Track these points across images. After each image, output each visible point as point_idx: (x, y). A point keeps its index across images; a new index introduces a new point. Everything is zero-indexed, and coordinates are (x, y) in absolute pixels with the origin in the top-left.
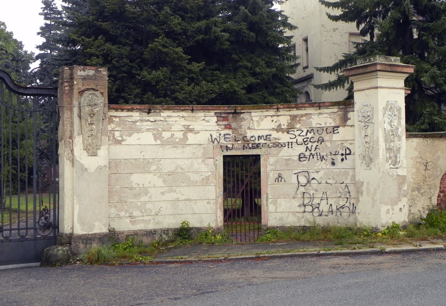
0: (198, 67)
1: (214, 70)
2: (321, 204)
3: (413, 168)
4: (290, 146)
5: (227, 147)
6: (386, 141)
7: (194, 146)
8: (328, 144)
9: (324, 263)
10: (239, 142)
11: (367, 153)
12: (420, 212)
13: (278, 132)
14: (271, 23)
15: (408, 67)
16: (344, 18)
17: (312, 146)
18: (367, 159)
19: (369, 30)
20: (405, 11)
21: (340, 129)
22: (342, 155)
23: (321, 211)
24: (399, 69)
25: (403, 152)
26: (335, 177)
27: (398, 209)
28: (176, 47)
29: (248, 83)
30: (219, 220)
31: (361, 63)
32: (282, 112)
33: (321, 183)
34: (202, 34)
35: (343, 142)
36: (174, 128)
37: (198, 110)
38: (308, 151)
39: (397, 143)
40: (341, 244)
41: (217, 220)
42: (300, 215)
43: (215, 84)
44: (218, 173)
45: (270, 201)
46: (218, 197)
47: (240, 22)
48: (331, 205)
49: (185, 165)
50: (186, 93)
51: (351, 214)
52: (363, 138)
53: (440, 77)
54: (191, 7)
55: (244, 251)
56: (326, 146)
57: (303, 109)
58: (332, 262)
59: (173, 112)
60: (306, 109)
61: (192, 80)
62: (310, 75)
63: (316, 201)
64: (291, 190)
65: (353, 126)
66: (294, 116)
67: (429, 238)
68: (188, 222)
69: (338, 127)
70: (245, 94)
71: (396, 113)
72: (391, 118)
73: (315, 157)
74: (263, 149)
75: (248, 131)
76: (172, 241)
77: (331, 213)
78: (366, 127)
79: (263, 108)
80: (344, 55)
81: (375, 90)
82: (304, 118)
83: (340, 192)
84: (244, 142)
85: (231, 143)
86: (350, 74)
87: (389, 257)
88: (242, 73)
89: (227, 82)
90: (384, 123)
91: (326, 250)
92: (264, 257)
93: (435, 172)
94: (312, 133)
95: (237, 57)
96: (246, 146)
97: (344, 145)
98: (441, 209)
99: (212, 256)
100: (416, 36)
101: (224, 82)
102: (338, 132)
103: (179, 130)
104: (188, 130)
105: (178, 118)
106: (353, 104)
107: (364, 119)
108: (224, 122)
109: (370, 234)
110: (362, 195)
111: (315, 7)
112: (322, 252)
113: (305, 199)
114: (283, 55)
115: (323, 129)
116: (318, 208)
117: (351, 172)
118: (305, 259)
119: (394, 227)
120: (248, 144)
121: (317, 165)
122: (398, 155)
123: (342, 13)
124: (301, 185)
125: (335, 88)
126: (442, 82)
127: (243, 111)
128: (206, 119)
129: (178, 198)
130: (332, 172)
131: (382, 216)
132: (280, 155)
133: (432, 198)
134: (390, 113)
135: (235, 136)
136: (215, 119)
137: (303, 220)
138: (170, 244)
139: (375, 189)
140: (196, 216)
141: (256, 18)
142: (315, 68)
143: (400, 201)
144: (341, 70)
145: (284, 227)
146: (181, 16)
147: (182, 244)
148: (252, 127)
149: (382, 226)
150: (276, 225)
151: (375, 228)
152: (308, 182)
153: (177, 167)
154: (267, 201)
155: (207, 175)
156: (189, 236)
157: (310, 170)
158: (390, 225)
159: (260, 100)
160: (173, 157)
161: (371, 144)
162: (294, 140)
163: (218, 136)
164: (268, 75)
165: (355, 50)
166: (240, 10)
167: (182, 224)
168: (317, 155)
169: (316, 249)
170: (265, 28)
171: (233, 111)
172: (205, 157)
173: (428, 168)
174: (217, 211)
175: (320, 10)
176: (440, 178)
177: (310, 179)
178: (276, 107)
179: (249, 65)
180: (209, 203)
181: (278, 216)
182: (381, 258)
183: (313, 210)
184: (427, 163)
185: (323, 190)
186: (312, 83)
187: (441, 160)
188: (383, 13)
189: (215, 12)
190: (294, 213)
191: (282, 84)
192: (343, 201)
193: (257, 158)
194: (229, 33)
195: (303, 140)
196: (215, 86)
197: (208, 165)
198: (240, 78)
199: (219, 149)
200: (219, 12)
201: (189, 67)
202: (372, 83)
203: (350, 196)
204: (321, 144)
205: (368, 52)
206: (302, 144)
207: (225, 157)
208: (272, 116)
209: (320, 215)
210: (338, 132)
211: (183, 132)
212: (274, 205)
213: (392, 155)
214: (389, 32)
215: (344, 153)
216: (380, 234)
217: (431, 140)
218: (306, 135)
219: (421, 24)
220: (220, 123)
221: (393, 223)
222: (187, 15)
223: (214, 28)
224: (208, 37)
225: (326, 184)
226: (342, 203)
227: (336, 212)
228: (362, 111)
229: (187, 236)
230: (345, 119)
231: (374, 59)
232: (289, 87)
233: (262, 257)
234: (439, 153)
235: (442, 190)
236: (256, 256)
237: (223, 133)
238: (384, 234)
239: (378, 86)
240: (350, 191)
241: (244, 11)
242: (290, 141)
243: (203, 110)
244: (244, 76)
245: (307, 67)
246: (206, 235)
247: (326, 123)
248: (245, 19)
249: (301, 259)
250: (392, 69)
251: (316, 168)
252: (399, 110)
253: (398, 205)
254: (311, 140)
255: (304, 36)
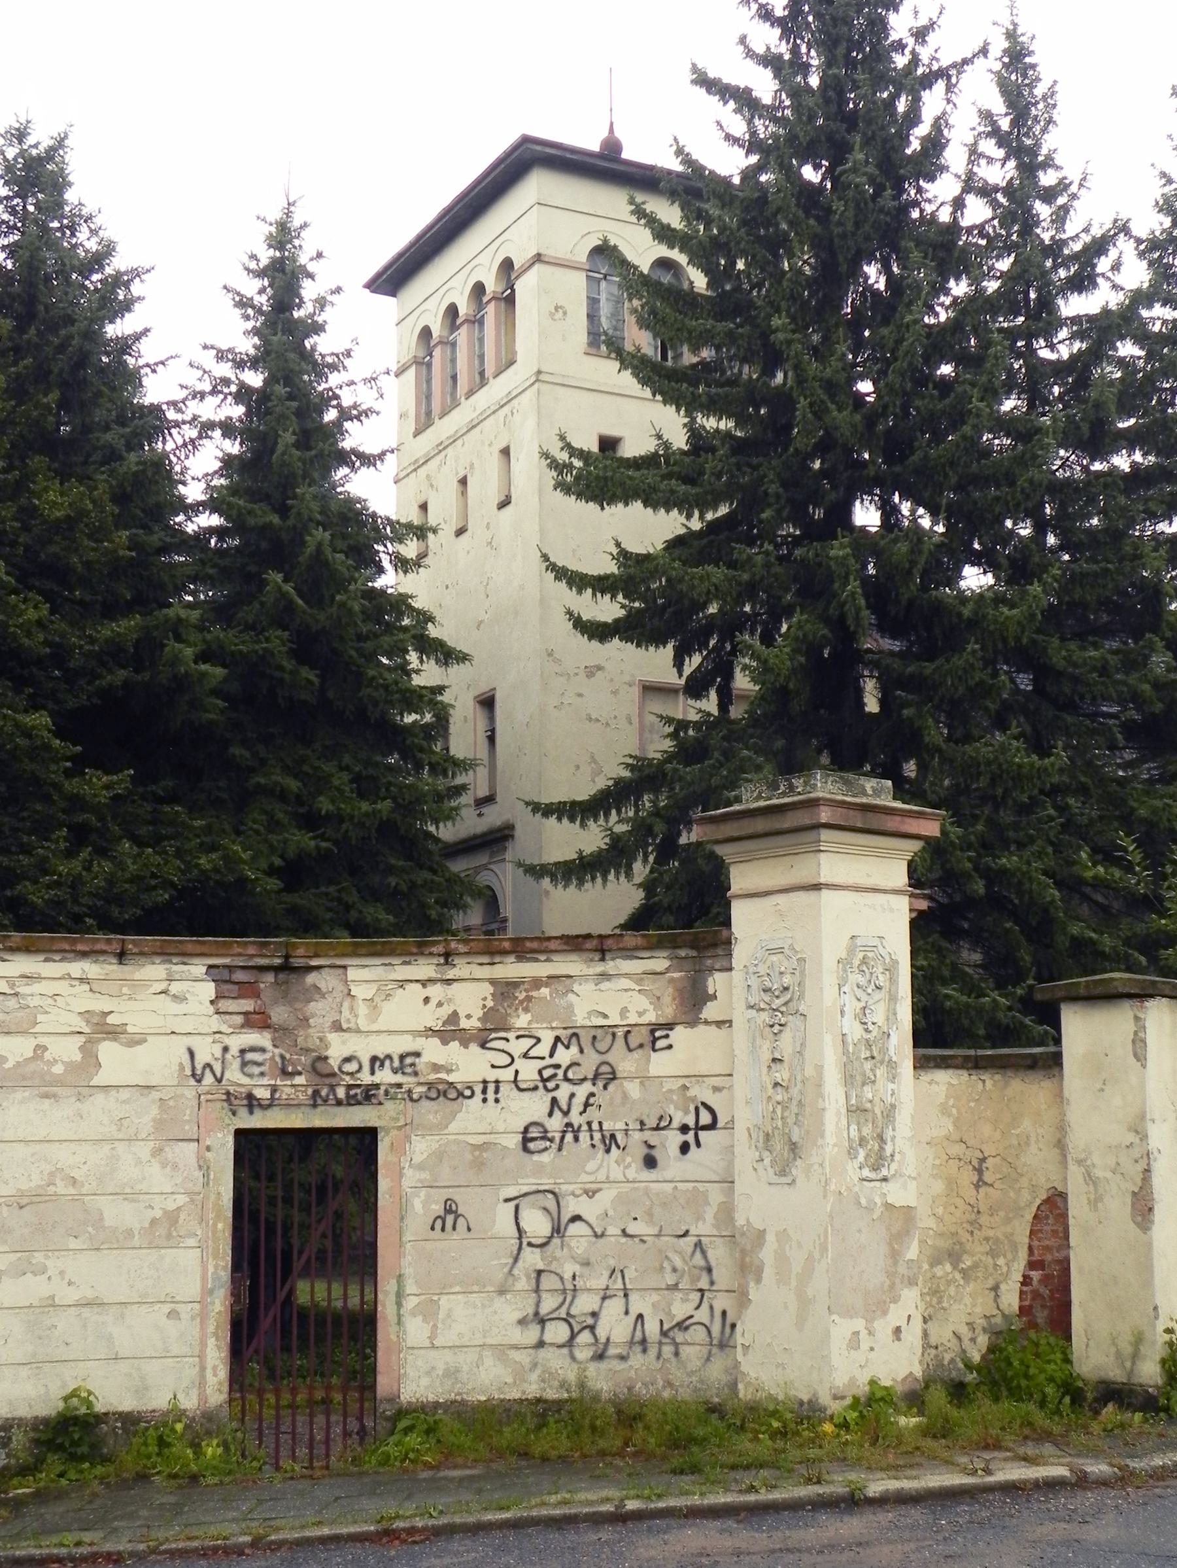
0: (107, 787)
1: (161, 800)
2: (603, 1314)
3: (934, 1176)
4: (491, 1095)
5: (250, 1097)
6: (848, 1079)
7: (125, 1094)
8: (633, 1089)
9: (652, 1553)
10: (300, 1080)
11: (780, 1123)
12: (959, 1338)
13: (445, 1042)
14: (376, 636)
15: (920, 815)
16: (628, 629)
17: (572, 1095)
18: (778, 1144)
19: (713, 678)
20: (842, 618)
21: (679, 1035)
22: (684, 1129)
23: (603, 1340)
24: (892, 823)
25: (904, 1118)
26: (657, 1210)
27: (889, 1332)
28: (26, 711)
29: (291, 852)
30: (211, 1380)
31: (759, 797)
32: (461, 968)
33: (603, 1235)
34: (124, 667)
35: (686, 1082)
36: (46, 1023)
37: (142, 954)
38: (557, 1114)
39: (884, 1087)
40: (695, 1469)
41: (202, 1384)
42: (523, 1357)
43: (166, 853)
44: (213, 1197)
45: (410, 1303)
46: (211, 1292)
47: (263, 630)
48: (640, 1316)
49: (85, 1168)
50: (58, 884)
51: (715, 1350)
52: (765, 1070)
53: (962, 850)
54: (88, 564)
55: (326, 1506)
56: (625, 1096)
57: (542, 957)
58: (678, 1548)
59: (46, 960)
60: (555, 957)
61: (80, 836)
62: (500, 829)
63: (584, 1304)
64: (494, 1263)
65: (723, 1022)
66: (508, 984)
67: (1008, 1440)
68: (90, 1393)
69: (670, 1026)
70: (279, 892)
71: (881, 978)
72: (864, 997)
73: (584, 1136)
74: (389, 1105)
75: (333, 1037)
76: (25, 1471)
77: (638, 1349)
78: (777, 1028)
79: (392, 953)
80: (630, 761)
81: (811, 896)
82: (545, 991)
83: (674, 1270)
84: (317, 1080)
85: (265, 1081)
86: (720, 837)
87: (885, 1517)
88: (266, 813)
89: (213, 848)
90: (842, 1013)
91: (649, 1498)
92: (412, 1531)
93: (1012, 1194)
94: (574, 1049)
95: (247, 754)
96: (324, 1093)
97: (691, 1093)
98: (1033, 1325)
99: (196, 1532)
100: (872, 705)
101: (202, 844)
102: (670, 1047)
103: (68, 1030)
104: (103, 1029)
105: (66, 983)
106: (728, 942)
107: (767, 998)
108: (243, 1001)
109: (791, 1427)
110: (759, 1280)
111: (522, 587)
112: (632, 1505)
113: (544, 1295)
114: (419, 755)
115: (614, 1035)
116: (592, 1328)
117: (716, 1195)
118: (571, 1537)
119: (877, 1401)
120: (332, 1088)
121: (591, 1166)
122: (889, 1134)
123: (623, 612)
124: (530, 1244)
125: (599, 880)
126: (969, 865)
127: (314, 962)
128: (175, 988)
129: (53, 1297)
130: (647, 1192)
131: (835, 1360)
132: (453, 1127)
133: (1003, 1287)
134: (862, 981)
135: (282, 1057)
136: (209, 989)
137: (534, 1377)
138: (15, 1481)
139: (810, 1259)
140: (123, 1367)
141: (321, 618)
142: (527, 804)
143: (895, 1300)
144: (619, 812)
145: (463, 1403)
146: (49, 597)
147: (64, 1482)
148: (348, 1021)
149: (835, 1397)
150: (431, 1398)
151: (810, 1401)
152: (558, 1230)
153: (51, 1174)
154: (399, 1305)
155: (171, 1205)
156: (93, 1446)
157: (564, 1188)
158: (863, 1389)
159: (329, 915)
160: (41, 1134)
161: (795, 1092)
162: (507, 1075)
163: (218, 1054)
164: (362, 825)
165: (668, 745)
166: (263, 583)
167: (66, 1399)
168: (590, 1129)
169: (605, 1493)
170: (353, 653)
171: (278, 961)
172: (166, 1135)
173: (988, 1177)
174: (203, 1345)
175: (542, 601)
176: (1029, 1217)
177: (565, 1217)
178: (440, 949)
179: (293, 785)
180: (173, 1315)
181: (441, 1361)
182: (853, 1526)
183: (573, 1336)
184: (983, 1160)
185: (612, 1262)
186: (509, 855)
187: (1033, 1148)
188: (764, 623)
189: (170, 587)
190: (501, 1350)
191: (409, 858)
192: (684, 1300)
193: (368, 1137)
194: (224, 666)
195: (540, 1072)
196: (166, 862)
197: (175, 1167)
198: (257, 832)
199: (219, 1105)
200: (181, 589)
201: (72, 786)
202: (800, 870)
203: (712, 1283)
204: (605, 1087)
205: (716, 754)
206: (536, 1088)
207: (240, 1134)
208: (424, 983)
209: (600, 1356)
210: (670, 1047)
211: (81, 1039)
212: (425, 1320)
213: (867, 1130)
214: (791, 686)
215: (692, 1124)
216: (828, 1427)
217: (997, 1077)
218: (551, 1056)
219: (897, 664)
220: (224, 1005)
221: (873, 1382)
222: (71, 591)
223: (172, 646)
224: (146, 676)
225: (624, 1240)
226: (680, 1310)
227: (660, 1343)
228: (762, 969)
229: (84, 1449)
230: (693, 1000)
231: (806, 783)
232: (434, 872)
233: (404, 1529)
234: (1026, 1125)
235: (1036, 1257)
236: (380, 1527)
237: (237, 1042)
238: (844, 1425)
239: (822, 880)
240: (713, 1263)
241: (280, 588)
242: (492, 1075)
243: (164, 954)
244: (274, 825)
245: (490, 799)
246: (162, 1443)
247: (624, 1012)
248: (284, 615)
249: (554, 1536)
250: (866, 823)
251: (584, 1178)
252: (891, 969)
253: (890, 1316)
254: (570, 1075)
255: (483, 688)
